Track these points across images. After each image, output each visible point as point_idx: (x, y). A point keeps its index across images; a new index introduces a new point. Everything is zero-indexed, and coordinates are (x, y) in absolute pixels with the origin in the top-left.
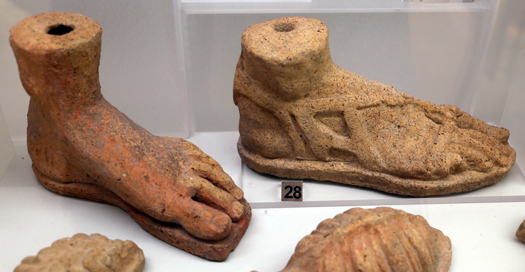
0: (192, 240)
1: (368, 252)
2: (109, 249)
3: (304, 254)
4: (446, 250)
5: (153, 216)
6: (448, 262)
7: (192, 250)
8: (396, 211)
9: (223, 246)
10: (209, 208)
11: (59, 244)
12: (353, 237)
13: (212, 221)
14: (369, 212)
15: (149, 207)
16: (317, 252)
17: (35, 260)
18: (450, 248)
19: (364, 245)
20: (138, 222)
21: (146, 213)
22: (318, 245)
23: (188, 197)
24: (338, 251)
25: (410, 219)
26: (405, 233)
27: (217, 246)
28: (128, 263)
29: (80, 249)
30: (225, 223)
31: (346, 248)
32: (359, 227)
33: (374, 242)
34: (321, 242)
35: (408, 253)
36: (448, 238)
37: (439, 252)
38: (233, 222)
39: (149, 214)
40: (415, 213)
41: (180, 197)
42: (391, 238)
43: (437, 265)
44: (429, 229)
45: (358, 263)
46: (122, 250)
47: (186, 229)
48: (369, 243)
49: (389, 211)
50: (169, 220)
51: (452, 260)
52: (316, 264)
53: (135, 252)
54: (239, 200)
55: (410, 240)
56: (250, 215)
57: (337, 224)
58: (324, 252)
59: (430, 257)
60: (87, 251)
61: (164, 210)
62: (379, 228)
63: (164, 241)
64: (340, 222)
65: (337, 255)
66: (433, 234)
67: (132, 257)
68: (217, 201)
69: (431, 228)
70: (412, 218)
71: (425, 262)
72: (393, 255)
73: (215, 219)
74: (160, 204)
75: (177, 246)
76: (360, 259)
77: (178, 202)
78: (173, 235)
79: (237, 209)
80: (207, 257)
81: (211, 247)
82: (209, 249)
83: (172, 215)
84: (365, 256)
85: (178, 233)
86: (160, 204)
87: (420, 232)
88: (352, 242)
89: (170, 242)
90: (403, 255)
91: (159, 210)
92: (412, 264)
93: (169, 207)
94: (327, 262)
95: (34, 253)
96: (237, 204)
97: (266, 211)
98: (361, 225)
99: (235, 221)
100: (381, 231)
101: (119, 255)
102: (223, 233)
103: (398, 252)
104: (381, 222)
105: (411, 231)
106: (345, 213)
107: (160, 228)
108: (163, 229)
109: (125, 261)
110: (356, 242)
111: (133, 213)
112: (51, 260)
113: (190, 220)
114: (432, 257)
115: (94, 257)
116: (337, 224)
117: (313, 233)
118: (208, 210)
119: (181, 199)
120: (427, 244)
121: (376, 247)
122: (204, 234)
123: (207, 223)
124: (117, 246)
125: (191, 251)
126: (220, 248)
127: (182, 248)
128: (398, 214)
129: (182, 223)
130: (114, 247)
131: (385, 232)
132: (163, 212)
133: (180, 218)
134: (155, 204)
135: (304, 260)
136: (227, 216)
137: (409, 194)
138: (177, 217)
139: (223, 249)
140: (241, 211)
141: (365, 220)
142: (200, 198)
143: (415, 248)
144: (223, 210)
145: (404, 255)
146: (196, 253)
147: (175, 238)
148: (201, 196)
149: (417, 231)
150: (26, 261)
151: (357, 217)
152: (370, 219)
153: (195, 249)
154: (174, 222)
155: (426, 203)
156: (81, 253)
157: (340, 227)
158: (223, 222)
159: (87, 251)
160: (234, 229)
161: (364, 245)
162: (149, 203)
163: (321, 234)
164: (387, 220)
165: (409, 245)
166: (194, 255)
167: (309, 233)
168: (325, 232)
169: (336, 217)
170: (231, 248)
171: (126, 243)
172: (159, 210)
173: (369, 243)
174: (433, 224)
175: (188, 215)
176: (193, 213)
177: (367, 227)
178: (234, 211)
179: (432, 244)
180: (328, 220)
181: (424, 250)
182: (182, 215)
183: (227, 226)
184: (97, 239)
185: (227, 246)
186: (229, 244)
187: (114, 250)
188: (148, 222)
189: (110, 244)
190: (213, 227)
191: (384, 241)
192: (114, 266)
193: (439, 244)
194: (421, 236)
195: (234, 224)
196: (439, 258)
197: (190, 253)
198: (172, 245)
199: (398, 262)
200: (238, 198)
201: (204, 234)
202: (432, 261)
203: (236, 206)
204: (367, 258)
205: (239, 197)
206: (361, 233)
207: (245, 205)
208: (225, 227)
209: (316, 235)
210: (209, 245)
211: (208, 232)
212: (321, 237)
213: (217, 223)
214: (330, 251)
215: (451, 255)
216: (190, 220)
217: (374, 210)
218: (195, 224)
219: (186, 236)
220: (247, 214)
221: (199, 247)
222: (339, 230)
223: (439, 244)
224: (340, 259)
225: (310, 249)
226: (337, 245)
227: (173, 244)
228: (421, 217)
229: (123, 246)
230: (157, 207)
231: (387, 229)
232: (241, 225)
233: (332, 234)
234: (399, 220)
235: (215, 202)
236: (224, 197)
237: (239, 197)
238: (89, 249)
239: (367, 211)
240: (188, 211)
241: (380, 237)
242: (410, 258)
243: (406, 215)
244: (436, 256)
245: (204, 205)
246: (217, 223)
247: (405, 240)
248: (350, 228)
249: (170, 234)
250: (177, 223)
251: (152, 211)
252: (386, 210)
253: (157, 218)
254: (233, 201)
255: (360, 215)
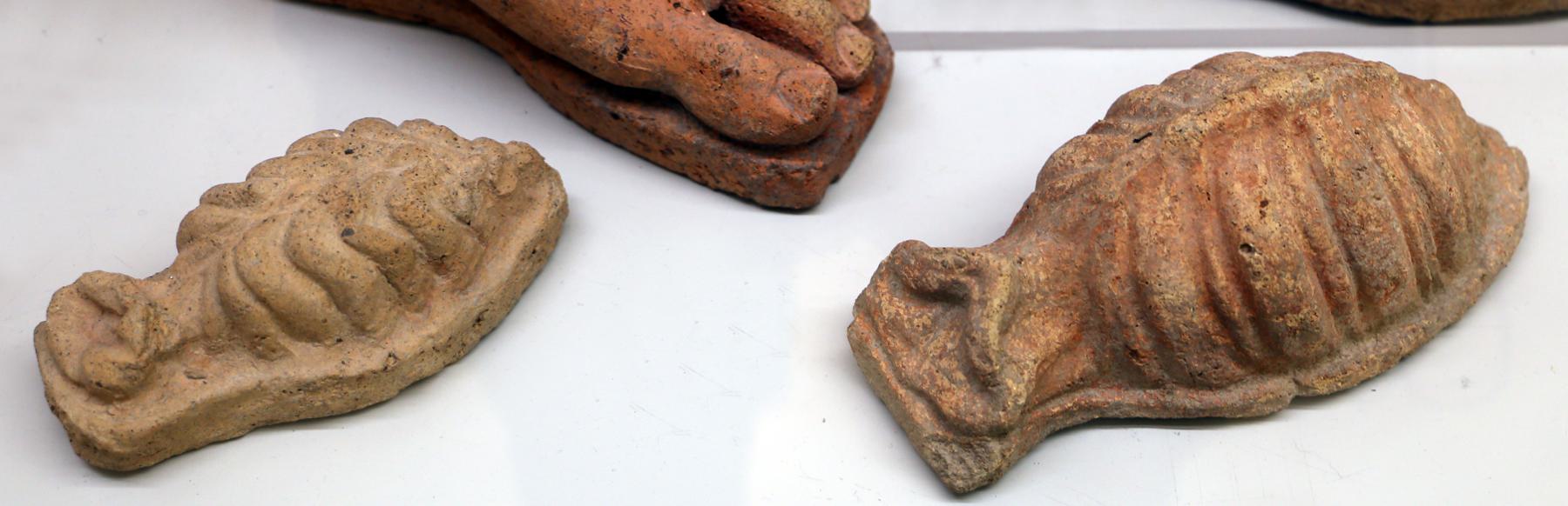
0: (713, 144)
1: (1272, 190)
2: (462, 168)
3: (1072, 192)
4: (1512, 190)
5: (588, 70)
6: (1516, 227)
7: (711, 174)
8: (1366, 65)
9: (808, 163)
10: (766, 45)
11: (316, 148)
12: (1229, 144)
13: (777, 87)
14: (1280, 66)
15: (577, 40)
16: (1113, 188)
17: (245, 195)
18: (1523, 186)
19: (1262, 170)
20: (535, 87)
21: (567, 58)
22: (1116, 165)
23: (698, 10)
24: (1178, 186)
25: (1407, 90)
26: (1390, 134)
27: (789, 164)
28: (519, 212)
29: (376, 167)
30: (819, 93)
31: (1202, 178)
32: (1246, 114)
33: (1292, 161)
34: (1124, 158)
35: (1395, 195)
36: (1519, 153)
37: (1490, 197)
38: (841, 91)
39: (575, 63)
40: (1423, 75)
41: (674, 12)
42: (1347, 147)
43: (1482, 236)
44: (1464, 125)
45: (1242, 223)
46: (501, 171)
47: (695, 111)
48: (1279, 162)
49: (1345, 65)
50: (639, 82)
51: (1529, 221)
52: (1107, 224)
53: (539, 178)
54: (856, 24)
55: (1404, 155)
56: (889, 71)
57: (1178, 101)
58: (1133, 186)
59: (1463, 211)
60: (396, 171)
61: (625, 51)
62: (1310, 116)
63: (620, 146)
64: (1187, 98)
65: (1175, 198)
66: (1476, 139)
67: (529, 192)
68: (791, 23)
69: (1471, 121)
70: (1413, 87)
71: (1446, 226)
72: (1350, 203)
73: (783, 80)
74: (611, 30)
75: (662, 160)
76: (1248, 212)
77: (667, 25)
78: (651, 129)
79: (852, 50)
80: (758, 199)
81: (773, 166)
82: (764, 173)
83: (651, 65)
84: (1264, 203)
85: (666, 123)
86: (611, 30)
87: (1436, 132)
88: (1224, 159)
89: (640, 149)
90: (1381, 203)
91: (610, 49)
92: (1408, 229)
93: (639, 40)
94: (1144, 219)
95: (236, 175)
96: (851, 37)
97: (937, 62)
98: (1255, 108)
99: (847, 87)
100: (1317, 126)
101: (493, 185)
102: (810, 122)
103: (1368, 191)
104: (1316, 101)
105: (1410, 128)
106: (1198, 67)
107: (609, 106)
108: (621, 109)
109: (510, 204)
110: (1236, 158)
111: (522, 59)
112: (291, 197)
113: (707, 82)
114: (1467, 210)
115: (420, 189)
116: (1178, 101)
117: (1096, 128)
118: (762, 52)
119: (678, 16)
120: (1456, 172)
121: (1297, 176)
122: (751, 125)
123: (762, 92)
124: (484, 158)
125: (707, 177)
126: (799, 171)
127: (678, 168)
128: (1371, 77)
129: (682, 92)
130: (476, 162)
131: (1328, 130)
132: (620, 58)
133: (675, 75)
134: (596, 29)
135: (1072, 210)
136: (821, 71)
137: (1398, 13)
138: (666, 73)
139: (808, 173)
140: (863, 56)
141: (1267, 92)
142: (735, 15)
143: (1421, 182)
144: (811, 52)
145: (1386, 202)
146: (723, 185)
147: (659, 139)
148: (740, 8)
149: (1429, 128)
150: (214, 197)
151: (1241, 83)
152: (1282, 88)
153: (722, 173)
154: (655, 87)
155: (1430, 43)
156: (381, 177)
157: (1187, 111)
158: (811, 89)
159: (396, 171)
160: (843, 112)
161: (1262, 170)
162: (577, 29)
163: (1125, 132)
164: (1337, 92)
165: (1402, 172)
166: (717, 190)
167: (1082, 129)
168: (1137, 126)
169: (1170, 81)
170: (831, 171)
171: (511, 150)
172: (610, 49)
173: (1279, 162)
174: (1479, 109)
175: (701, 68)
176: (716, 62)
177: (1273, 113)
178: (843, 58)
179: (1471, 172)
180: (1144, 89)
181: (1444, 183)
182: (680, 67)
183: (823, 102)
184: (424, 137)
185: (821, 164)
186: (829, 159)
187: (477, 169)
188: (570, 88)
189: (464, 151)
190: (781, 107)
191: (1326, 159)
192: (480, 218)
193: (1490, 172)
194: (1440, 144)
195: (842, 98)
196: (1487, 214)
197: (704, 184)
198: (647, 160)
199: (1363, 222)
200: (853, 17)
201: (751, 128)
202: (1469, 221)
203: (848, 40)
204: (1268, 210)
205: (856, 11)
206: (1252, 131)
207: (873, 39)
208: (817, 106)
209: (1106, 137)
210: (767, 161)
211: (763, 120)
212: (1126, 141)
213: (790, 93)
214: (1155, 186)
215: (1527, 206)
216: (707, 82)
217: (1295, 61)
218: (723, 94)
219: (693, 131)
220: (882, 67)
221: (734, 165)
222: (1183, 121)
223: (1490, 172)
224: (1184, 212)
225: (1092, 179)
226: (1175, 167)
227: (651, 156)
228: (1441, 85)
229: (503, 159)
230: (601, 39)
231: (1335, 119)
232: (863, 103)
233: (1162, 132)
234: (1372, 94)
235: (783, 27)
236: (812, 13)
237: (856, 11)
238: (403, 166)
239: (1273, 64)
240: (701, 56)
241: (1311, 146)
242: (1401, 210)
243: (1396, 79)
244: (1480, 208)
245: (752, 38)
246: (790, 93)
247: (1390, 155)
248: (1220, 115)
249: (642, 123)
250: (663, 90)
251: (585, 53)
252: (1332, 61)
253: (603, 75)
254: (839, 26)
255: (1256, 75)
